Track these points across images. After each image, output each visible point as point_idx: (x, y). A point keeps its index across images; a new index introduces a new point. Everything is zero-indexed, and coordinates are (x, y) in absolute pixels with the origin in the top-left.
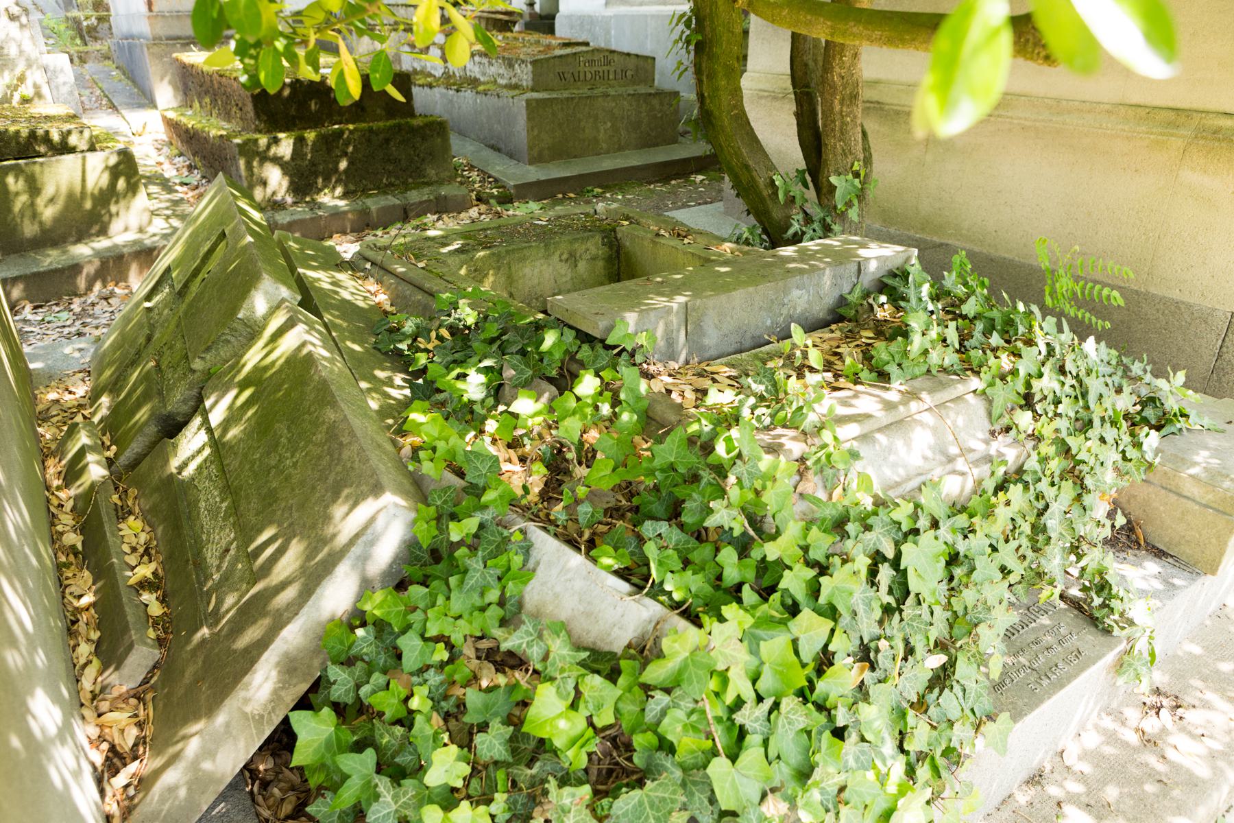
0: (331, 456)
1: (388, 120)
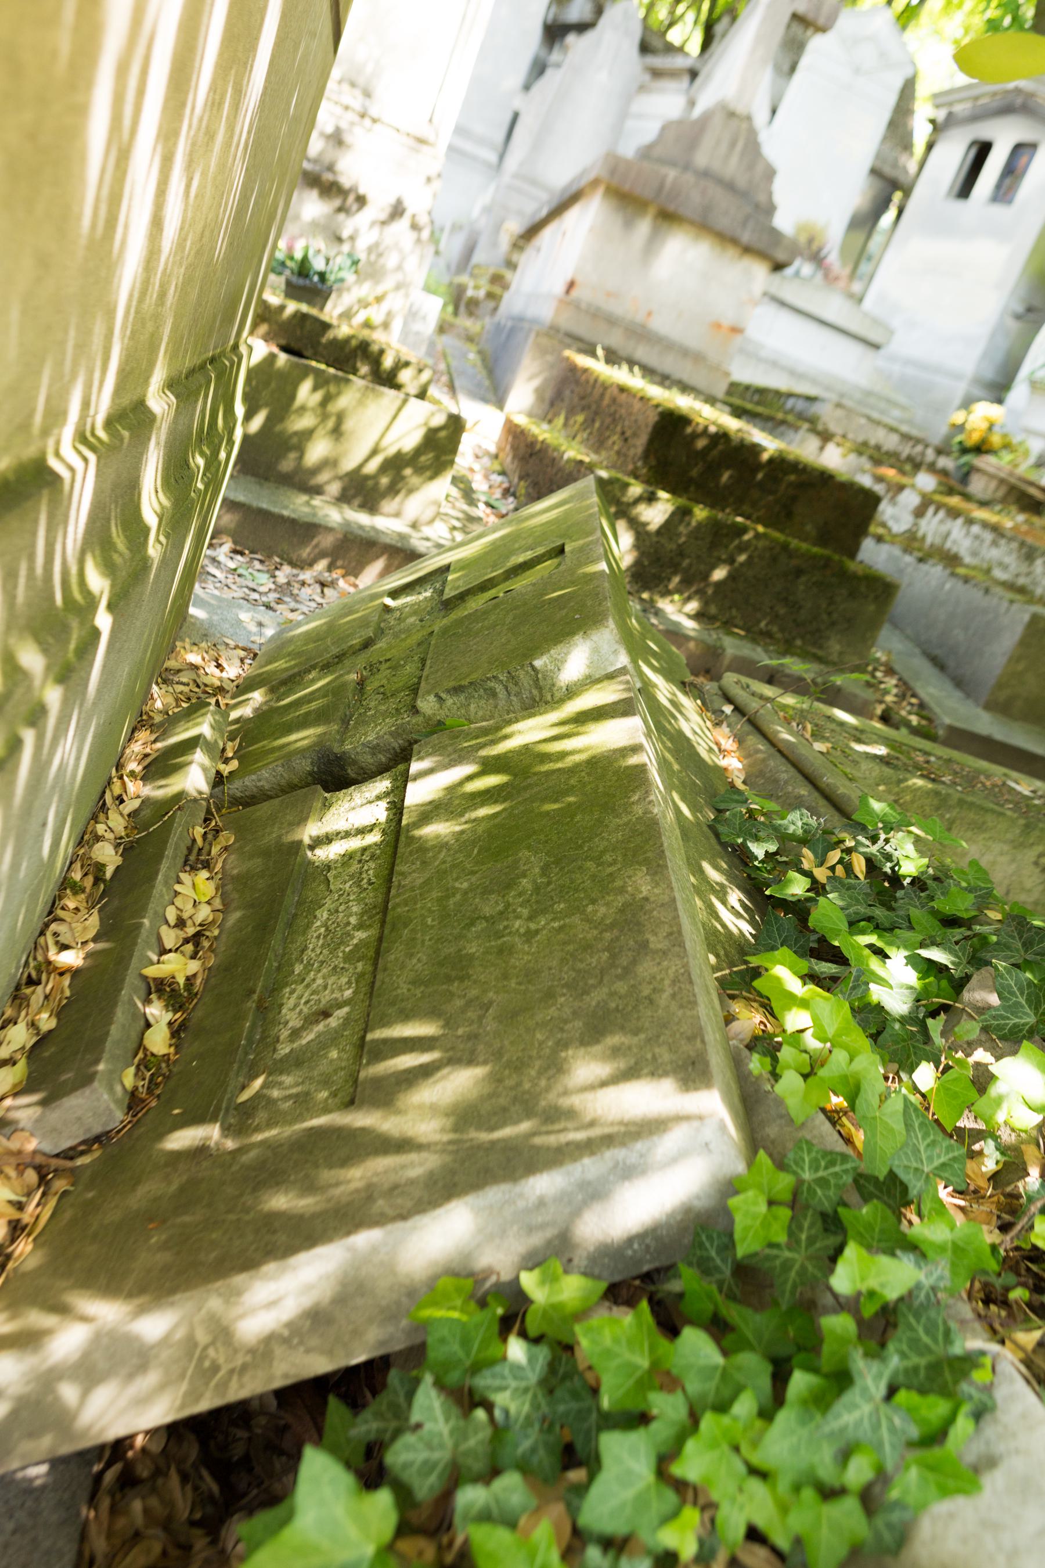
0: (613, 956)
1: (815, 545)
